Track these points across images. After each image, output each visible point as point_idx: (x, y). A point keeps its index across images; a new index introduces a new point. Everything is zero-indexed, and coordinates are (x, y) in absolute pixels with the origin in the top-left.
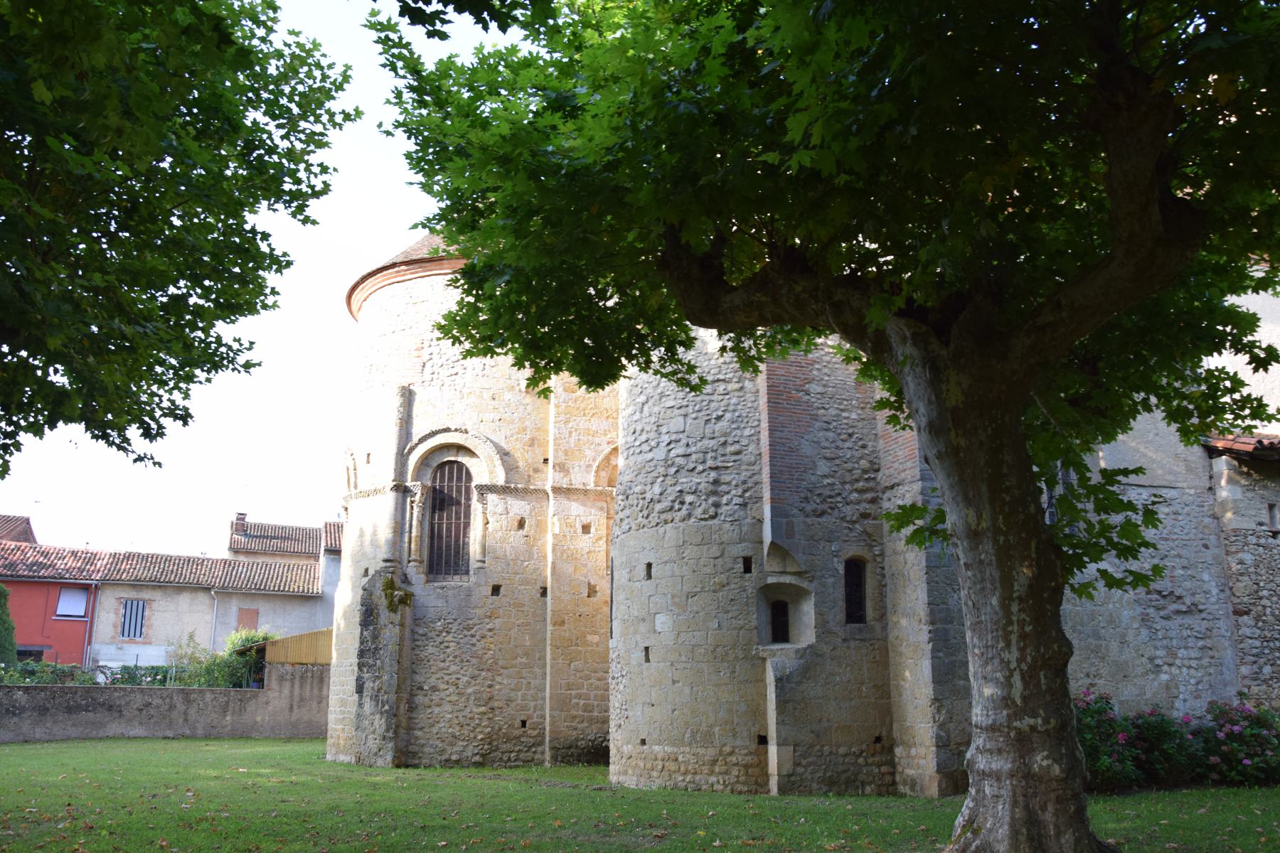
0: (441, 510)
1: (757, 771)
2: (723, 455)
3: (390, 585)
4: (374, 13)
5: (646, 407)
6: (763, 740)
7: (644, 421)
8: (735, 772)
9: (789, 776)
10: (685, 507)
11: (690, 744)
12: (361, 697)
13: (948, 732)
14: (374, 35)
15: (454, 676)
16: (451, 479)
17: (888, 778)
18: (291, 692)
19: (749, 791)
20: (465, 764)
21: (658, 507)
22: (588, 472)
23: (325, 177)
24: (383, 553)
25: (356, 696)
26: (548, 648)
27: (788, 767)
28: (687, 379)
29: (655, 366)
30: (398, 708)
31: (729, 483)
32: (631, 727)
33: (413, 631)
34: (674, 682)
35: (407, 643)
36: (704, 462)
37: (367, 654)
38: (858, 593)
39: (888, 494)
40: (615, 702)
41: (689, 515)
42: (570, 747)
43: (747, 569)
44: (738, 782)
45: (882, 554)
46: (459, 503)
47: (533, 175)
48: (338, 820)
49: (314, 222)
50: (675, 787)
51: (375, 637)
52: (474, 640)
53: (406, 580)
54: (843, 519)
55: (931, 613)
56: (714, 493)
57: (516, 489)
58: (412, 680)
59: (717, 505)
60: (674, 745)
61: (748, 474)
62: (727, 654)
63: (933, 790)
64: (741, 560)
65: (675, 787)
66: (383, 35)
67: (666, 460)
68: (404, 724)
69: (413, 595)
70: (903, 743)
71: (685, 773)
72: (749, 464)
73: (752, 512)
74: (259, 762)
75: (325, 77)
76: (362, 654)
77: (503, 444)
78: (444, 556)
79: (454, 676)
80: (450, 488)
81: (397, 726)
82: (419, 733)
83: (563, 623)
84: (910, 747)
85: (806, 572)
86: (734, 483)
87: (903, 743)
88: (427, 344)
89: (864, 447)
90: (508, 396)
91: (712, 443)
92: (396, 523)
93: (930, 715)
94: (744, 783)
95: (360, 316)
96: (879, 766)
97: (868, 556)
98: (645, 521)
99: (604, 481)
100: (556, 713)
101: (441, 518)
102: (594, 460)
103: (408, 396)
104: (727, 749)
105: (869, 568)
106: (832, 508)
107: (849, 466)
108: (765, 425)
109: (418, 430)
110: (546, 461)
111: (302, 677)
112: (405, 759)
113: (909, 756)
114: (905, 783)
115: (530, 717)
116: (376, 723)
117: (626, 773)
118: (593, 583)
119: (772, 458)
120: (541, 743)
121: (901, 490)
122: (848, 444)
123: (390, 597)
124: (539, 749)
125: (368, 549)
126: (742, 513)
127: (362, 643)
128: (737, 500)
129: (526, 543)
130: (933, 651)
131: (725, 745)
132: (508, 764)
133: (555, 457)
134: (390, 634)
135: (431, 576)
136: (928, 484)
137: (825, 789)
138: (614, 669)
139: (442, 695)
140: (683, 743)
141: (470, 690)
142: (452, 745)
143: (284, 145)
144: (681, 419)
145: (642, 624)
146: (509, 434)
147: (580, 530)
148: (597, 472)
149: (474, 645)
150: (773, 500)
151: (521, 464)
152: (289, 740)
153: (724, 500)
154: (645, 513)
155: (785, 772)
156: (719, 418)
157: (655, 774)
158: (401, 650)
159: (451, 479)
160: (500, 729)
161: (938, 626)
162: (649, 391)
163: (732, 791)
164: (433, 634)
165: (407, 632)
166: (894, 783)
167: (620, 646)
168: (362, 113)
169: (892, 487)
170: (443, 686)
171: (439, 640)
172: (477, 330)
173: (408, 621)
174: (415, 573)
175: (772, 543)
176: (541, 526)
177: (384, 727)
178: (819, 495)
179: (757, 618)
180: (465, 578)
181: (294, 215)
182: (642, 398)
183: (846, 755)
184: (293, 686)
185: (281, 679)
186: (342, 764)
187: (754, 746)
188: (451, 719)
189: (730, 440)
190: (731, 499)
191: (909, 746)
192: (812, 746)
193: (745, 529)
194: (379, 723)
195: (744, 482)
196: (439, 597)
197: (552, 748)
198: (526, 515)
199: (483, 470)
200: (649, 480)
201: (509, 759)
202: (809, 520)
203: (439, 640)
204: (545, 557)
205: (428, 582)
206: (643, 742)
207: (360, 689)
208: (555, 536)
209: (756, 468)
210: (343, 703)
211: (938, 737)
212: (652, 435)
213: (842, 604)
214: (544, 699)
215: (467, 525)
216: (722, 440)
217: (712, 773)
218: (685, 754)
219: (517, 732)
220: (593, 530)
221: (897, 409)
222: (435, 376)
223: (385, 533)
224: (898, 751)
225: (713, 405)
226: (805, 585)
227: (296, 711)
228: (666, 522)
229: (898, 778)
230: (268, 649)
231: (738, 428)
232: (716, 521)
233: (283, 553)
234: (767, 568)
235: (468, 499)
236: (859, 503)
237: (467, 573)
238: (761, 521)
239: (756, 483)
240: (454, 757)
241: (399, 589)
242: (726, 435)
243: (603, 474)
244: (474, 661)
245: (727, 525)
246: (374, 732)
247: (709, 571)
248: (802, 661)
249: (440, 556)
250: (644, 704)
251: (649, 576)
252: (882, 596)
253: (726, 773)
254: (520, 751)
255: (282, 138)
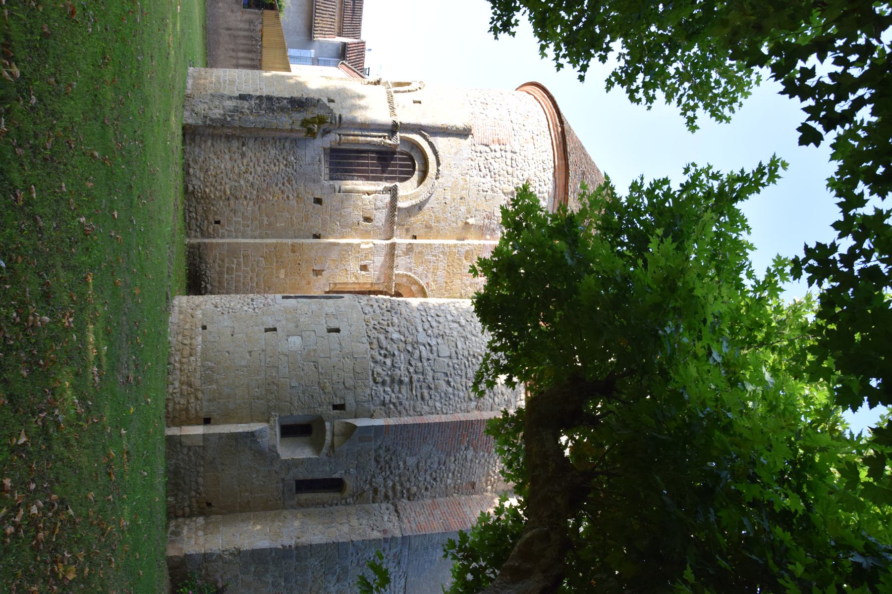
0: (379, 159)
1: (184, 417)
2: (421, 387)
3: (321, 121)
4: (785, 165)
5: (456, 325)
6: (207, 421)
7: (446, 324)
8: (183, 401)
9: (181, 444)
10: (382, 358)
11: (203, 366)
12: (236, 98)
13: (215, 561)
14: (766, 163)
15: (253, 170)
16: (402, 166)
17: (180, 512)
18: (241, 29)
19: (168, 412)
20: (187, 179)
21: (382, 337)
22: (406, 269)
23: (644, 100)
24: (346, 115)
25: (237, 94)
26: (274, 241)
27: (188, 442)
28: (482, 382)
29: (494, 356)
30: (229, 128)
31: (400, 392)
32: (215, 317)
33: (286, 138)
34: (250, 352)
35: (278, 134)
36: (416, 372)
37: (269, 103)
38: (318, 489)
39: (391, 507)
40: (234, 301)
41: (376, 362)
42: (200, 258)
43: (335, 407)
44: (175, 403)
45: (347, 504)
46: (383, 172)
47: (657, 307)
48: (136, 112)
49: (608, 89)
50: (171, 355)
51: (282, 109)
52: (280, 185)
53: (326, 132)
54: (373, 476)
55: (305, 547)
56: (393, 381)
57: (394, 216)
58: (249, 138)
59: (384, 383)
60: (202, 353)
61: (407, 406)
62: (272, 393)
63: (172, 552)
64: (343, 402)
65: (171, 355)
66: (766, 171)
67: (417, 342)
68: (216, 132)
69: (314, 138)
70: (207, 524)
71: (181, 363)
72: (414, 407)
73: (378, 409)
74: (187, 18)
75: (723, 105)
76: (269, 98)
77: (427, 206)
78: (346, 161)
79: (253, 170)
80: (395, 166)
81: (214, 127)
82: (209, 143)
83: (293, 251)
84: (204, 530)
85: (334, 451)
86: (400, 396)
87: (207, 524)
88: (503, 147)
89: (426, 489)
90: (463, 209)
91: (430, 378)
92: (369, 125)
93: (228, 547)
94: (174, 409)
95: (522, 94)
96: (189, 506)
97: (346, 494)
98: (371, 327)
99: (399, 281)
100: (226, 247)
101: (372, 158)
102: (415, 273)
103: (464, 133)
104: (200, 395)
105: (337, 495)
106: (381, 468)
107: (413, 479)
108: (443, 418)
109: (441, 142)
110: (415, 237)
111: (252, 37)
112: (190, 133)
113: (197, 529)
114: (177, 526)
115: (223, 227)
116: (217, 111)
117: (181, 312)
118: (324, 273)
119: (419, 425)
120: (203, 236)
121: (395, 519)
122: (428, 478)
123: (312, 121)
124: (199, 234)
125: (349, 102)
126: (378, 402)
127: (278, 99)
128: (387, 398)
129: (353, 223)
130: (276, 550)
131: (203, 393)
132: (187, 210)
133: (417, 245)
134: (285, 121)
135: (328, 151)
136: (399, 541)
137: (171, 468)
138: (259, 299)
139: (239, 162)
140: (204, 360)
141: (242, 182)
142: (201, 169)
143: (671, 70)
144: (448, 354)
145: (294, 325)
146: (435, 210)
147: (363, 263)
148: (406, 275)
149: (277, 185)
150: (387, 427)
151: (413, 219)
152: (205, 28)
153: (388, 389)
154: (378, 327)
155: (183, 440)
156: (448, 383)
157: (180, 338)
158: (272, 130)
159: (402, 166)
160: (213, 205)
161: (295, 552)
162: (469, 327)
163: (168, 399)
164: (285, 154)
165: (285, 134)
166: (177, 517)
167: (277, 306)
168: (693, 132)
169: (396, 511)
170: (245, 161)
171: (281, 158)
172: (520, 213)
173: (294, 135)
174: (331, 139)
175: (356, 427)
176: (366, 234)
177: (214, 117)
178: (391, 459)
179: (299, 414)
180: (327, 177)
181: (614, 74)
182: (463, 322)
183: (197, 483)
184: (245, 30)
185: (251, 22)
186: (185, 82)
187: (203, 415)
188: (220, 168)
189: (432, 392)
190: (388, 394)
191: (205, 529)
192: (203, 458)
193: (366, 405)
194: (217, 113)
195: (401, 404)
196: (313, 158)
197: (199, 244)
198: (374, 223)
199: (409, 191)
200: (402, 329)
201: (190, 212)
202: (372, 453)
203: (281, 158)
204: (343, 237)
205: (324, 149)
206: (204, 328)
207: (242, 97)
208: (359, 245)
209: (411, 412)
210: (232, 82)
211: (212, 555)
212: (436, 331)
213: (310, 477)
214: (237, 237)
215: (367, 179)
216: (432, 386)
217: (182, 383)
218: (196, 361)
219: (211, 218)
220: (363, 273)
221: (460, 547)
222: (479, 154)
223: (361, 116)
224: (201, 520)
225: (458, 378)
226: (324, 450)
227: (227, 32)
228: (371, 343)
229: (180, 520)
230: (273, 12)
231: (441, 398)
232: (372, 383)
233: (343, 10)
234: (336, 422)
235: (387, 179)
236: (385, 486)
237: (331, 179)
238: (372, 416)
239: (400, 413)
240: (191, 170)
241: (319, 128)
242: (436, 388)
243: (405, 280)
244: (265, 185)
245: (368, 392)
246: (210, 109)
247: (334, 378)
248: (267, 450)
249: (344, 158)
250: (233, 327)
251: (330, 331)
252: (316, 504)
253: (182, 394)
254: (197, 220)
255: (677, 69)
